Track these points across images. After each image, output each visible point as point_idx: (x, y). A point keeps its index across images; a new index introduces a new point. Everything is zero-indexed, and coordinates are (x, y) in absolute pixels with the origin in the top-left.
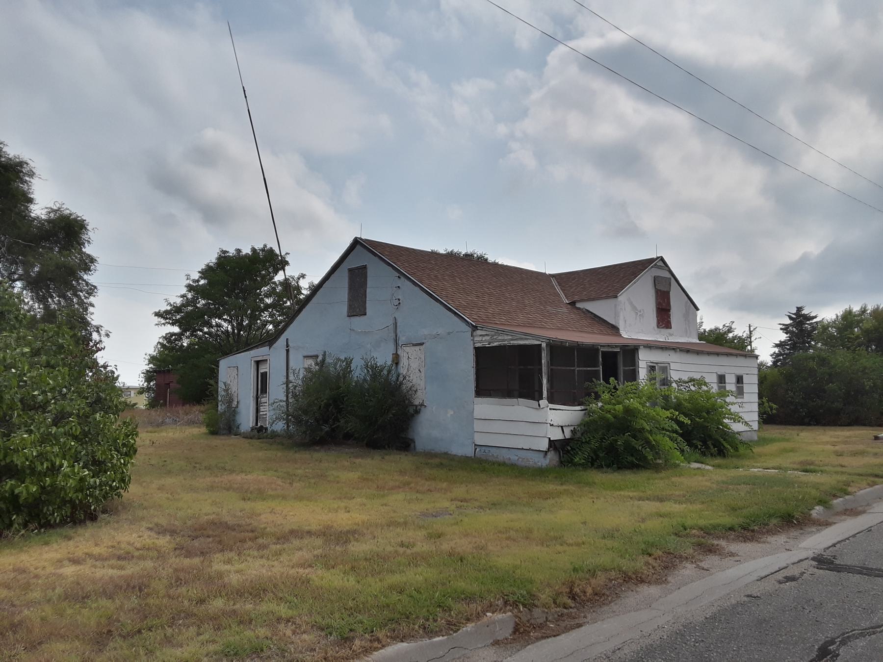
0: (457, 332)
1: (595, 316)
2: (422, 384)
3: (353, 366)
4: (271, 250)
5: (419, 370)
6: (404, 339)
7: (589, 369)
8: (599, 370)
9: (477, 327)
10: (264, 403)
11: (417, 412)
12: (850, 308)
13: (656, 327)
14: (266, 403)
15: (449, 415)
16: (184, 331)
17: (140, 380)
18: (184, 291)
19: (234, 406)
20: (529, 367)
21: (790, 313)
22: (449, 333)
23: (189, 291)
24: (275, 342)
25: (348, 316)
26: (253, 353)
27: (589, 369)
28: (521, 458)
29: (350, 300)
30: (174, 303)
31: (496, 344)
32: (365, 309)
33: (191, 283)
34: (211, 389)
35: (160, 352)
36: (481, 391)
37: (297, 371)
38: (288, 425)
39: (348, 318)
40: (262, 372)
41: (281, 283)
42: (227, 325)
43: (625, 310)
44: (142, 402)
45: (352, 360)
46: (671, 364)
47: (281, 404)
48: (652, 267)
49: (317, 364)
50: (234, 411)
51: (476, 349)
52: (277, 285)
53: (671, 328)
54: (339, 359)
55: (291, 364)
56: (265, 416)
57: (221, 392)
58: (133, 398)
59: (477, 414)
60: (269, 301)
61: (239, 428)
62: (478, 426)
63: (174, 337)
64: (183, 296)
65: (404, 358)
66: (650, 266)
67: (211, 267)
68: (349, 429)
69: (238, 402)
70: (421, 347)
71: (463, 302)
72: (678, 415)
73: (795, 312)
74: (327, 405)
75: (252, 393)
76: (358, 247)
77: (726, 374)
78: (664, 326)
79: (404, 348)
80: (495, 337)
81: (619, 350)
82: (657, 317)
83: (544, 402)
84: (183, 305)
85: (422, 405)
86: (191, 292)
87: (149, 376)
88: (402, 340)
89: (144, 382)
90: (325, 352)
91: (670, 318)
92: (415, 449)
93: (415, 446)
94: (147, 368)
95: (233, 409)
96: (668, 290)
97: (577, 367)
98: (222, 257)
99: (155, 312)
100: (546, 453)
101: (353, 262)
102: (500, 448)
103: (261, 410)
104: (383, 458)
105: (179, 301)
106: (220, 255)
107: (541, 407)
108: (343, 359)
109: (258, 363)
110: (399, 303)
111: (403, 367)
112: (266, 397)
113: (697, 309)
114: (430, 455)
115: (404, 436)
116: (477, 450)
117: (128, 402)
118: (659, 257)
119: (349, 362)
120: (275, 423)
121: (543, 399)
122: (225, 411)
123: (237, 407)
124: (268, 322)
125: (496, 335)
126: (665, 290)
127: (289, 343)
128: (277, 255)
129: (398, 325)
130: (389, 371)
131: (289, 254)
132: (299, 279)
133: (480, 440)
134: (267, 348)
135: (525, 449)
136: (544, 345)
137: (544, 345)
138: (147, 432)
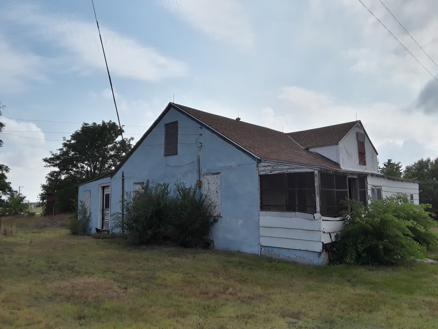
0: (245, 164)
1: (323, 157)
2: (219, 201)
3: (169, 189)
4: (114, 123)
5: (217, 192)
6: (205, 170)
7: (342, 190)
8: (347, 191)
9: (261, 160)
10: (108, 214)
11: (215, 221)
12: (422, 159)
13: (358, 164)
14: (109, 214)
15: (239, 224)
16: (62, 170)
17: (38, 199)
18: (61, 146)
19: (87, 216)
20: (304, 189)
21: (385, 163)
22: (239, 166)
23: (65, 146)
24: (115, 174)
25: (165, 156)
26: (100, 181)
27: (342, 190)
28: (299, 257)
29: (166, 144)
30: (56, 154)
31: (276, 172)
32: (177, 150)
33: (66, 142)
34: (73, 205)
35: (49, 184)
36: (263, 207)
37: (129, 193)
38: (123, 230)
39: (165, 157)
40: (106, 194)
41: (120, 143)
42: (87, 167)
43: (343, 153)
44: (39, 212)
45: (168, 186)
46: (382, 186)
47: (118, 215)
48: (355, 127)
49: (143, 188)
50: (88, 219)
51: (261, 176)
52: (117, 144)
53: (366, 165)
54: (159, 185)
55: (126, 189)
56: (108, 223)
57: (80, 208)
58: (33, 209)
59: (261, 224)
60: (112, 153)
61: (91, 230)
62: (262, 232)
63: (55, 174)
64: (61, 149)
65: (205, 183)
66: (354, 126)
67: (78, 133)
68: (167, 234)
69: (90, 213)
70: (218, 176)
71: (247, 144)
72: (416, 225)
73: (387, 162)
74: (151, 217)
75: (100, 207)
76: (172, 109)
77: (414, 194)
78: (362, 163)
79: (205, 177)
80: (275, 167)
81: (357, 177)
82: (359, 158)
83: (318, 215)
84: (61, 155)
85: (219, 216)
86: (65, 147)
87: (43, 197)
88: (204, 171)
89: (40, 200)
90: (148, 180)
91: (365, 159)
92: (214, 248)
93: (214, 245)
94: (42, 192)
95: (87, 218)
96: (364, 142)
97: (336, 189)
98: (85, 127)
99: (44, 159)
100: (320, 254)
101: (168, 119)
102: (281, 249)
103: (106, 219)
104: (194, 257)
105: (58, 153)
106: (84, 126)
107: (316, 219)
108: (163, 184)
109: (103, 188)
110: (202, 146)
111: (204, 190)
112: (109, 210)
113: (377, 154)
114: (229, 253)
115: (206, 238)
116: (263, 249)
117: (30, 212)
118: (358, 121)
119: (166, 186)
120: (114, 229)
121: (316, 213)
122: (82, 219)
123: (90, 216)
124: (111, 165)
125: (276, 166)
126: (362, 141)
127: (124, 175)
128: (117, 126)
129: (201, 160)
130: (195, 192)
131: (124, 126)
132: (130, 140)
133: (264, 242)
134: (109, 178)
135: (302, 250)
136: (316, 172)
137: (316, 172)
138: (33, 233)
